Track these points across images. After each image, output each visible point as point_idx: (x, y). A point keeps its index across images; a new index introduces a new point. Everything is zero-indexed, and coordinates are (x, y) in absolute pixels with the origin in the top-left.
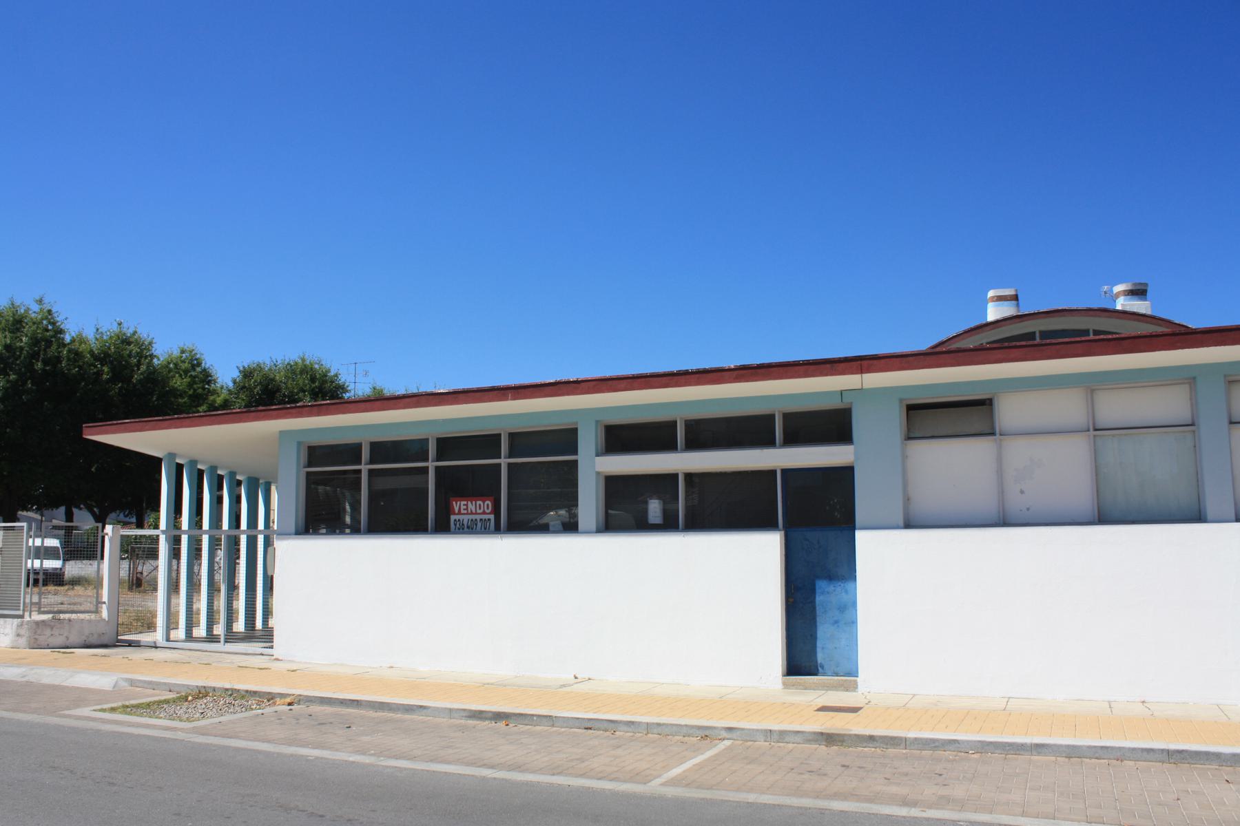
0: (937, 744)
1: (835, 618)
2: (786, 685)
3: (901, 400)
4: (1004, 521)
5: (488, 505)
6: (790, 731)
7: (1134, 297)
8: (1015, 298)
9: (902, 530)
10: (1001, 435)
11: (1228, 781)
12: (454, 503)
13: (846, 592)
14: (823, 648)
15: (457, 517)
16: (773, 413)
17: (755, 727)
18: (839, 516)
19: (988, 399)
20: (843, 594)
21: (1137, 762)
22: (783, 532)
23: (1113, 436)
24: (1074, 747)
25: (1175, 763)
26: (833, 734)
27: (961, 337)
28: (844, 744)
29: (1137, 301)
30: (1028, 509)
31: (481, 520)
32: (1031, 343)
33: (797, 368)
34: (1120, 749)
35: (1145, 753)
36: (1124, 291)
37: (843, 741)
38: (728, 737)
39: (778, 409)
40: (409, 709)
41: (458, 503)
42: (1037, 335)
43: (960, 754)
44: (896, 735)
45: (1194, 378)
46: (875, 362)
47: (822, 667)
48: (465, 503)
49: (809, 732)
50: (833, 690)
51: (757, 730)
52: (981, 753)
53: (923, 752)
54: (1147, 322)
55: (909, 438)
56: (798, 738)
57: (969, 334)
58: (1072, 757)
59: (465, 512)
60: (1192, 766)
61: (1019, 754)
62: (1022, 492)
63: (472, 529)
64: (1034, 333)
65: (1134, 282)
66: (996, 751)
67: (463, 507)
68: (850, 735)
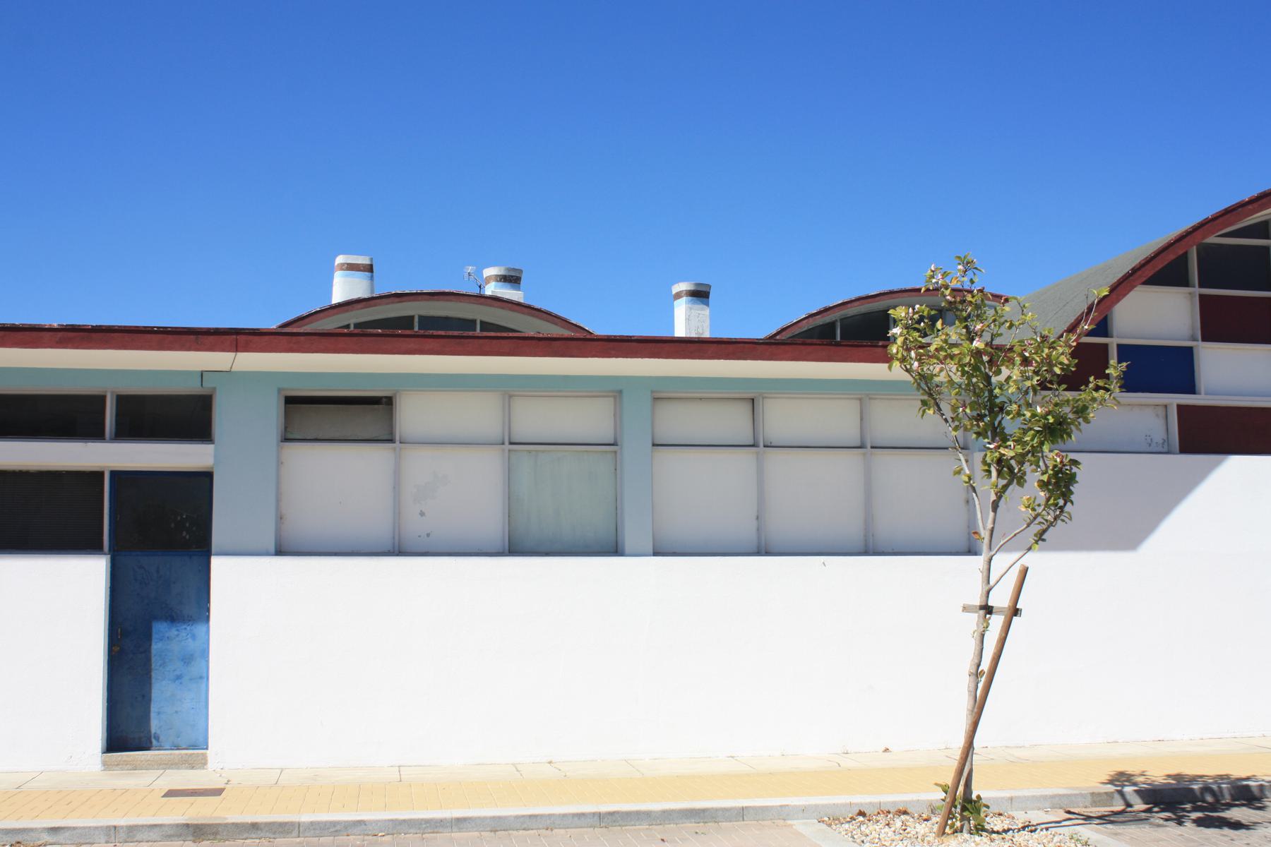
0: (338, 827)
1: (178, 673)
2: (106, 766)
3: (280, 390)
4: (398, 550)
6: (143, 826)
7: (507, 284)
8: (370, 268)
9: (274, 557)
10: (400, 443)
11: (663, 840)
13: (194, 637)
14: (159, 713)
16: (103, 394)
17: (91, 825)
18: (187, 537)
19: (386, 397)
20: (190, 640)
21: (567, 830)
22: (109, 556)
23: (529, 452)
24: (500, 818)
25: (606, 827)
26: (202, 825)
27: (326, 313)
28: (218, 837)
29: (509, 289)
30: (428, 535)
32: (408, 332)
33: (149, 336)
34: (550, 816)
35: (576, 819)
37: (216, 833)
38: (51, 841)
39: (111, 390)
42: (416, 320)
43: (366, 837)
44: (286, 820)
45: (620, 392)
46: (256, 338)
47: (157, 739)
49: (170, 825)
50: (172, 769)
51: (96, 828)
52: (393, 834)
53: (321, 839)
54: (543, 319)
55: (286, 439)
56: (154, 835)
58: (497, 831)
60: (624, 828)
61: (437, 833)
62: (422, 514)
64: (412, 318)
65: (507, 267)
66: (412, 831)
68: (226, 825)
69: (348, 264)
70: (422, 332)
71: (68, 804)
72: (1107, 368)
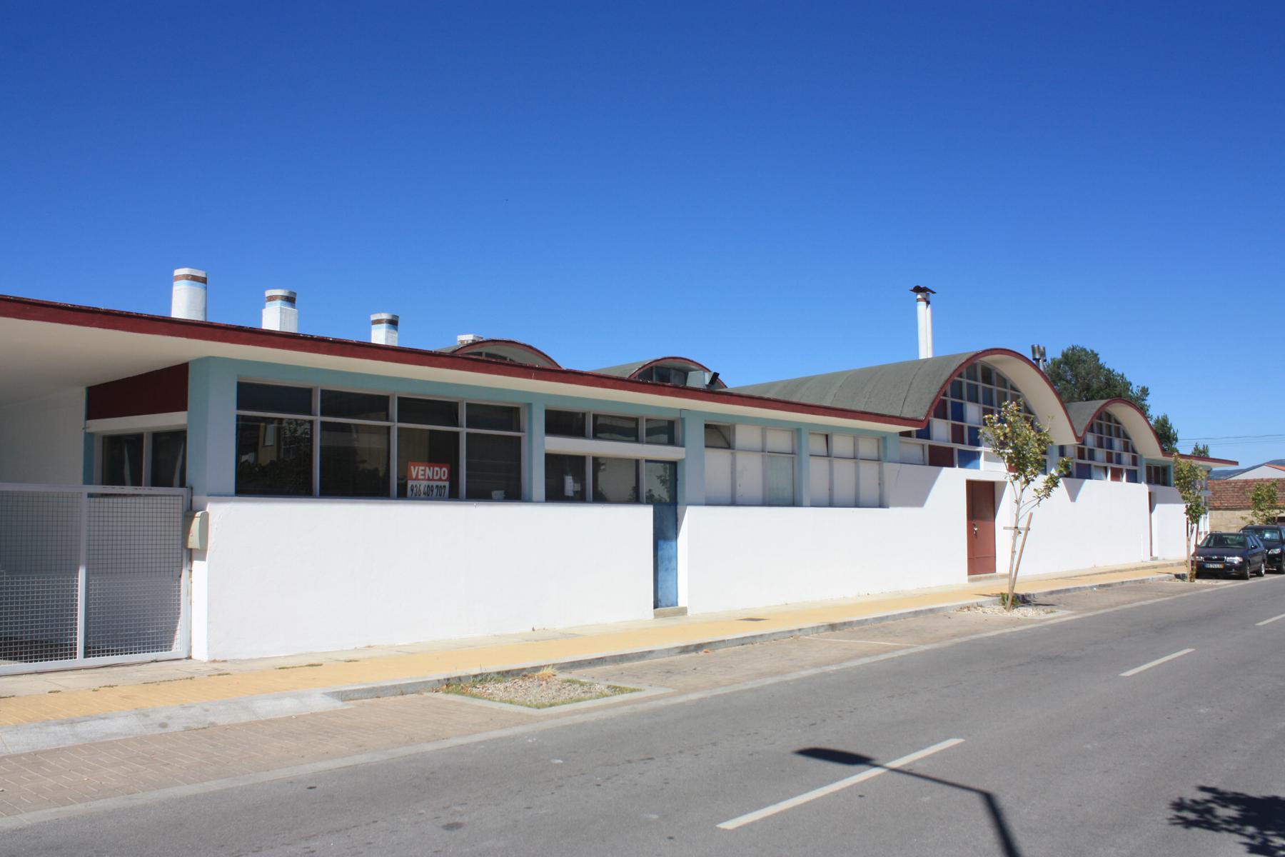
5: (444, 472)
8: (204, 281)
12: (412, 467)
15: (414, 483)
31: (437, 486)
36: (282, 296)
39: (319, 384)
40: (641, 656)
41: (417, 468)
48: (423, 468)
57: (471, 347)
59: (423, 477)
63: (428, 495)
67: (421, 473)
69: (192, 276)
70: (658, 383)
71: (124, 697)
72: (978, 435)
